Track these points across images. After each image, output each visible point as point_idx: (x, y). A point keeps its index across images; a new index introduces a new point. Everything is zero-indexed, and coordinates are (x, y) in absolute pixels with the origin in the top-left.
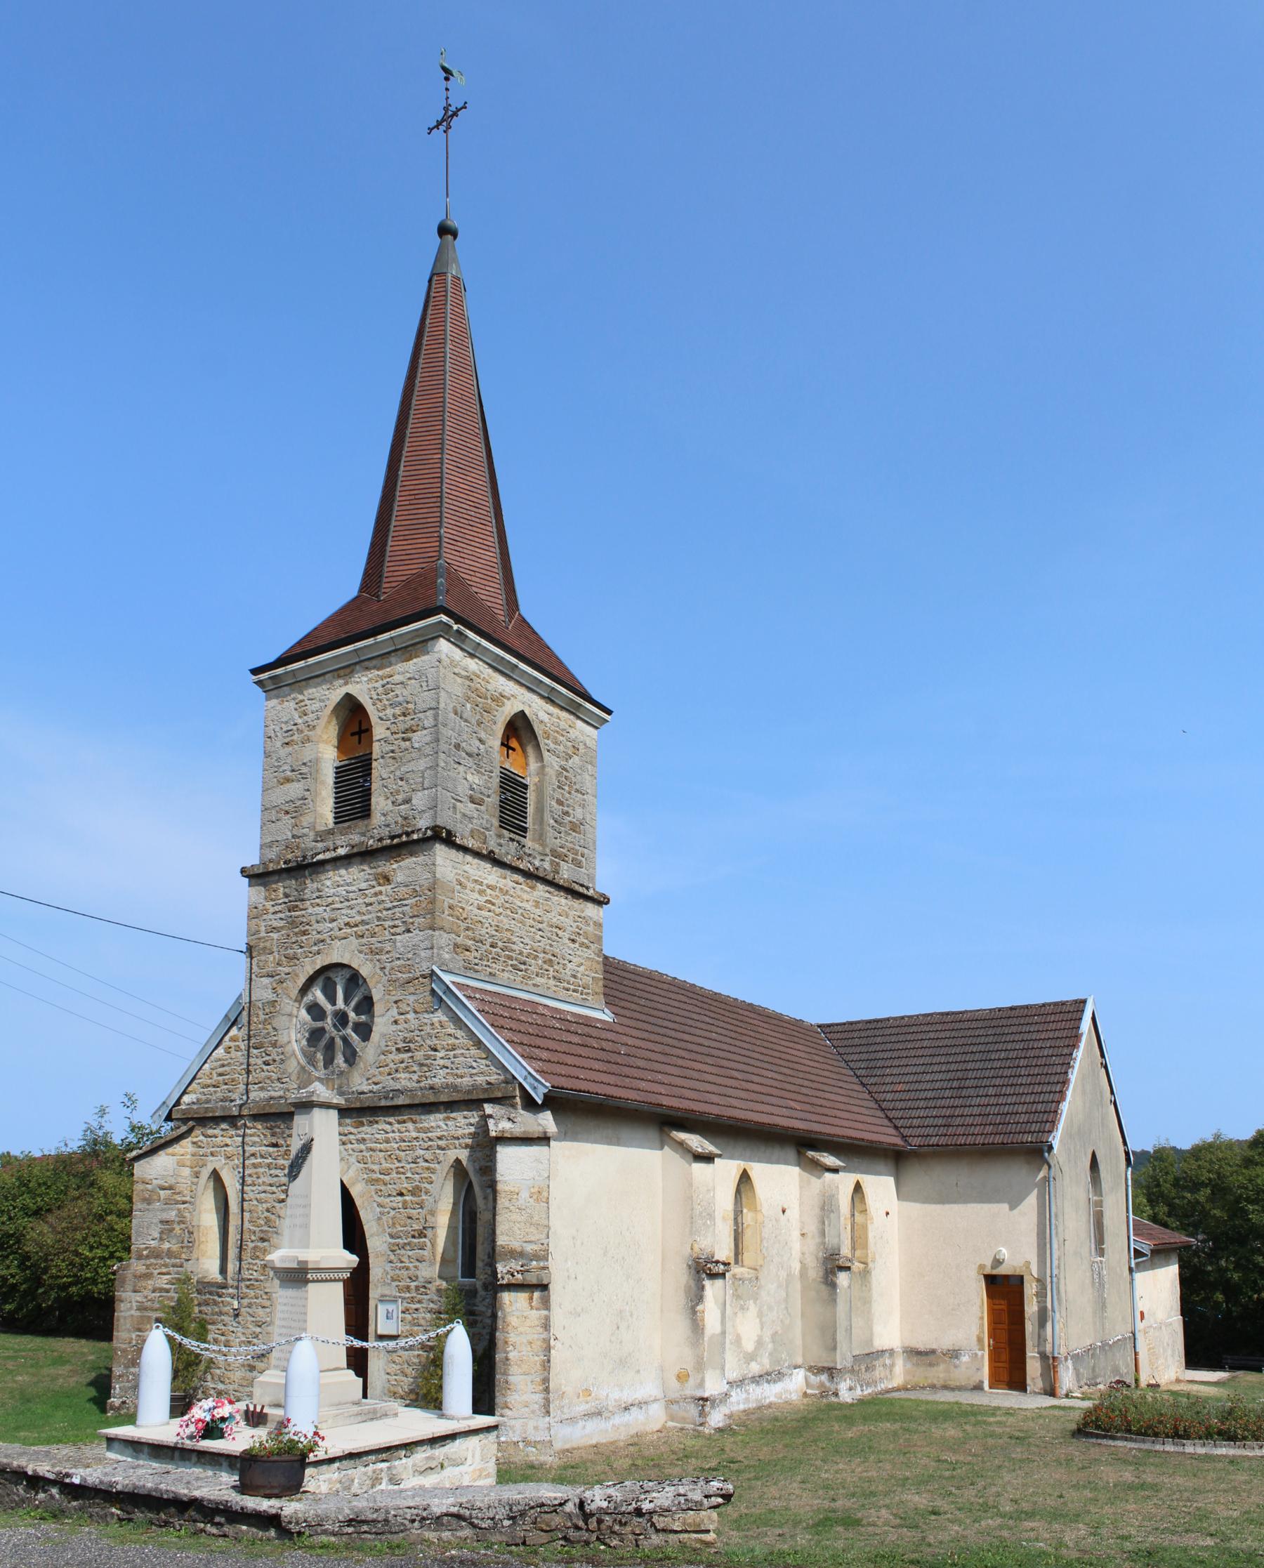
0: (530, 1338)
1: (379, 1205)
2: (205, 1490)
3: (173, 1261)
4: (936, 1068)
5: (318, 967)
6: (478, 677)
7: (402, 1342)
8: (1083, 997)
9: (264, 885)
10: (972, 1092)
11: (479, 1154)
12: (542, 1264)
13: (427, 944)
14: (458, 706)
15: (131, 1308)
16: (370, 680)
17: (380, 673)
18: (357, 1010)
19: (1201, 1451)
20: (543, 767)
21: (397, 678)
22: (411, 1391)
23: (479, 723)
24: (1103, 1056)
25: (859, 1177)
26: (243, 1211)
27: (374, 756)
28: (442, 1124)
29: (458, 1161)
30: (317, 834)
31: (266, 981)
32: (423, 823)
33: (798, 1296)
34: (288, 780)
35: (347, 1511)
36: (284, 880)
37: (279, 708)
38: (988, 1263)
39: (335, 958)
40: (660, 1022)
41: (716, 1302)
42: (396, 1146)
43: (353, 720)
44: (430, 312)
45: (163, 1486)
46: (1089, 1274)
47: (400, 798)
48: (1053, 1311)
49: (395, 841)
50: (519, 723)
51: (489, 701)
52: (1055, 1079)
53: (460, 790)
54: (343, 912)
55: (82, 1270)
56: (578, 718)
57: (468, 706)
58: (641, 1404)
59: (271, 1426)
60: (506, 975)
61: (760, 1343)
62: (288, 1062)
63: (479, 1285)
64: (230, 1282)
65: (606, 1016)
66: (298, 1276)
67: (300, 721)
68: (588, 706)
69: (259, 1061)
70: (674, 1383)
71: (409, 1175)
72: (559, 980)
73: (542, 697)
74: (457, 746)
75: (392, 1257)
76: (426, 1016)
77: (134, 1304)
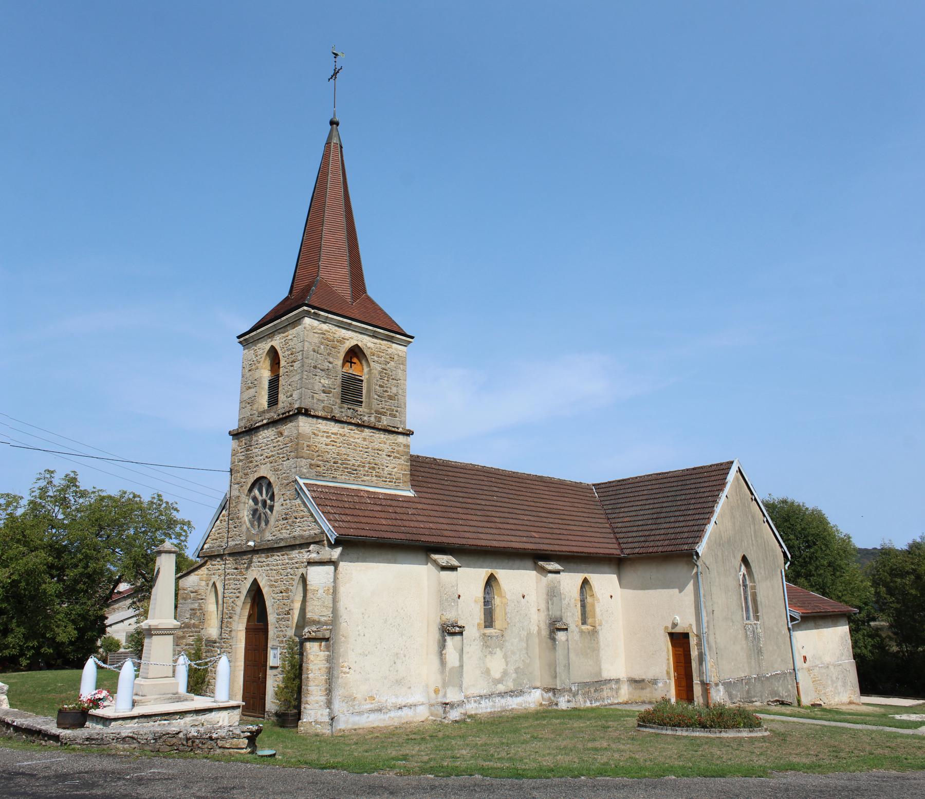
4: (647, 507)
19: (685, 734)
21: (290, 337)
23: (329, 354)
25: (586, 575)
31: (236, 486)
34: (250, 388)
38: (670, 625)
52: (707, 510)
53: (316, 388)
61: (505, 673)
65: (410, 494)
68: (398, 336)
70: (433, 695)
74: (315, 367)
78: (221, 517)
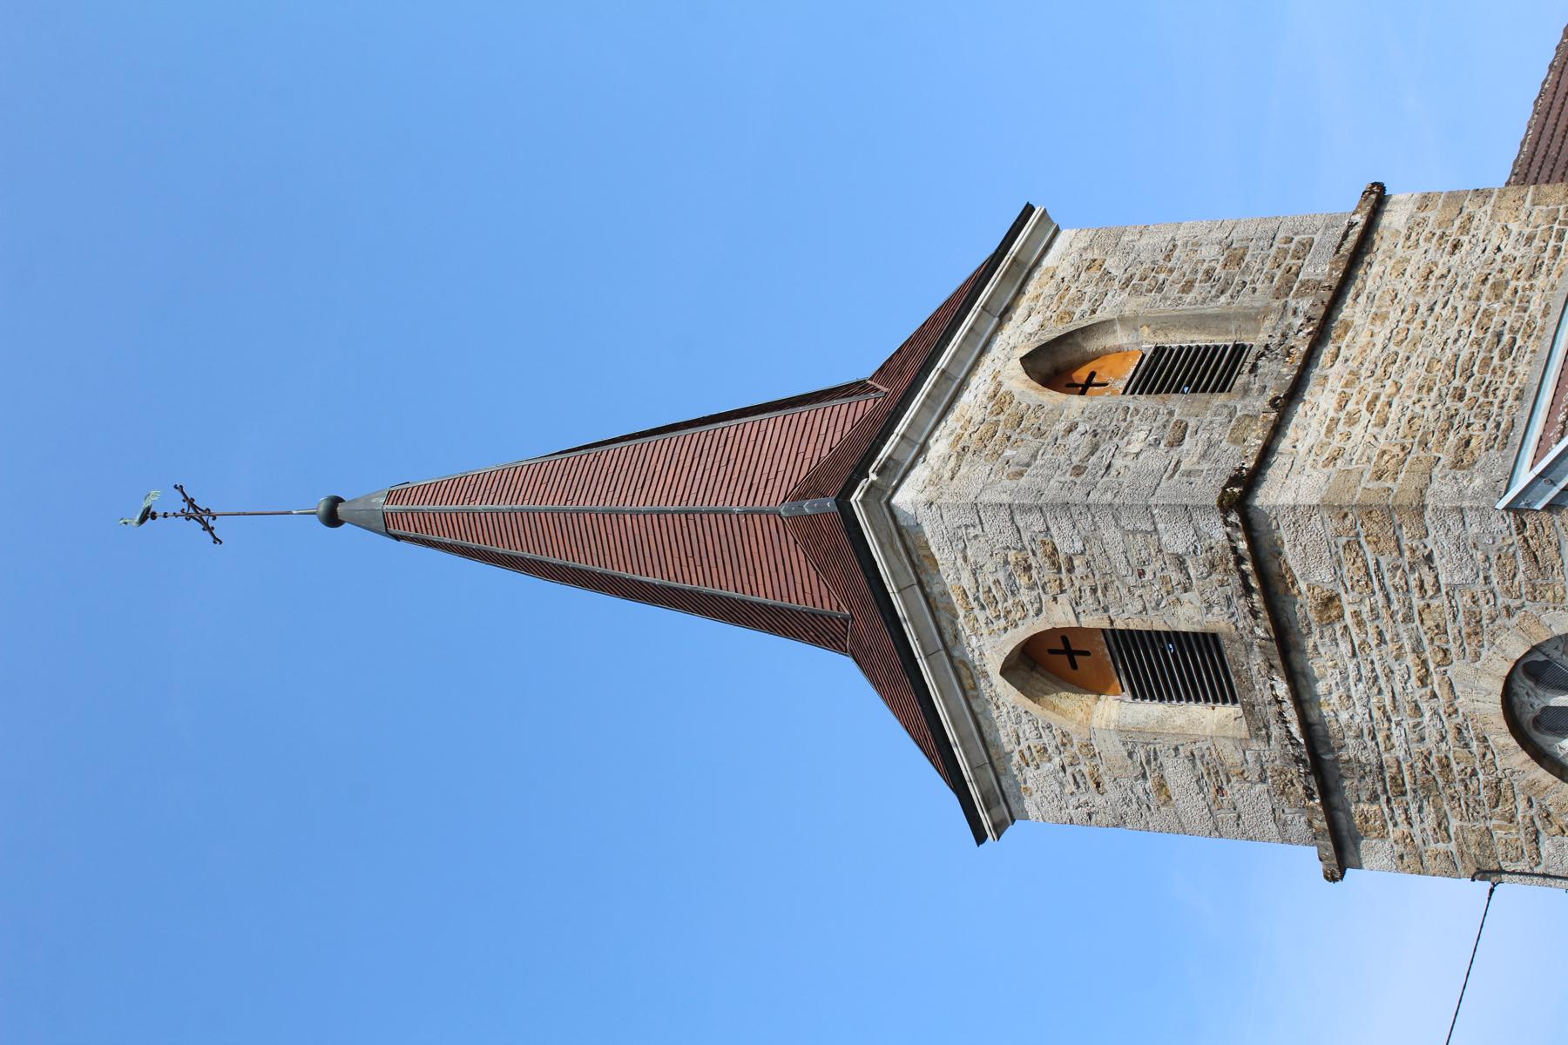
5: (1512, 742)
6: (960, 437)
9: (1357, 839)
14: (1008, 470)
16: (975, 631)
17: (961, 613)
20: (1123, 320)
21: (967, 581)
23: (1040, 433)
27: (1106, 625)
31: (1546, 847)
32: (1217, 531)
34: (1162, 786)
37: (1037, 796)
39: (1492, 708)
43: (1047, 662)
44: (435, 538)
47: (1176, 576)
49: (1254, 584)
50: (1045, 366)
51: (1002, 417)
54: (1398, 689)
57: (1008, 453)
60: (1521, 369)
67: (1057, 760)
72: (1537, 267)
73: (999, 327)
74: (1078, 470)
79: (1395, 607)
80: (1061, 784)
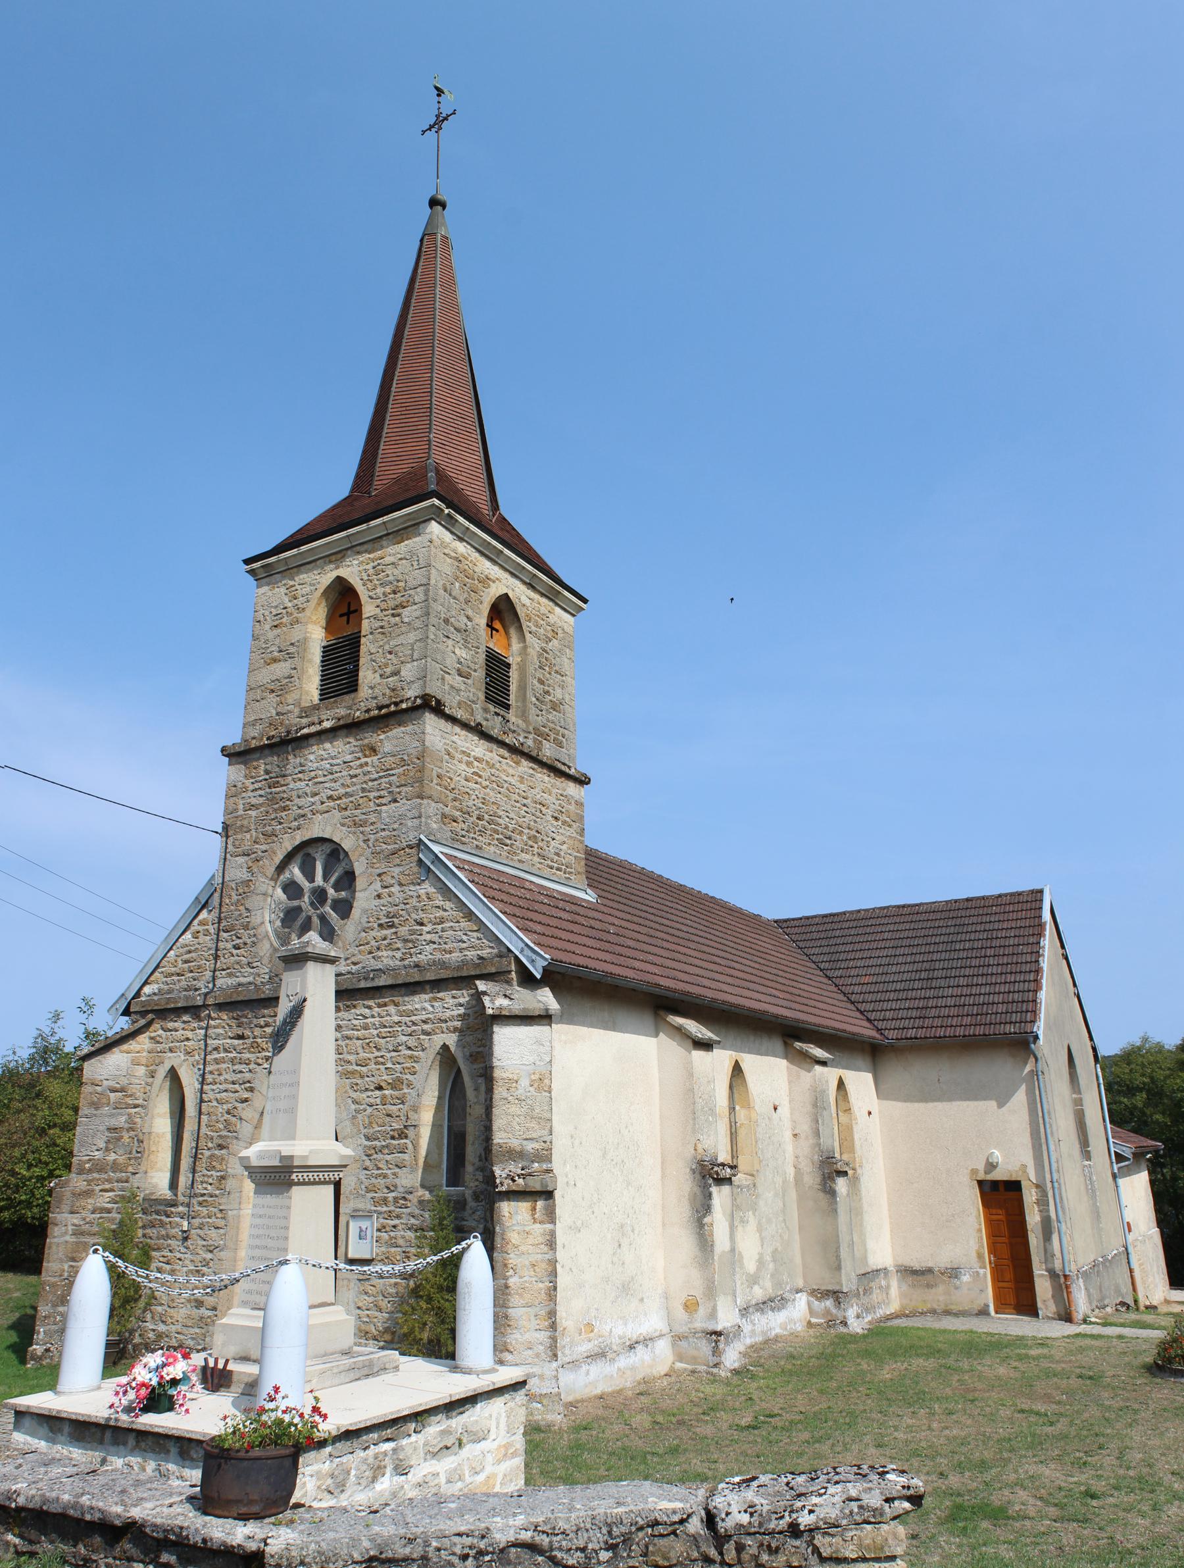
0: (533, 1258)
1: (355, 1102)
2: (149, 1505)
3: (119, 1175)
4: (900, 960)
5: (297, 843)
6: (466, 559)
7: (378, 1268)
8: (1038, 887)
9: (245, 763)
10: (943, 983)
11: (469, 1039)
12: (545, 1166)
13: (415, 813)
15: (66, 1233)
17: (371, 556)
18: (337, 887)
20: (525, 647)
21: (388, 560)
22: (387, 1330)
23: (467, 602)
24: (1063, 947)
26: (200, 1113)
27: (363, 633)
28: (427, 1005)
29: (445, 1047)
30: (303, 710)
31: (241, 860)
32: (412, 692)
33: (795, 1207)
34: (275, 660)
35: (366, 1544)
36: (266, 757)
37: (270, 593)
38: (981, 1167)
39: (316, 833)
40: (639, 906)
41: (724, 1214)
42: (375, 1032)
43: (344, 602)
45: (85, 1500)
46: (1082, 1179)
47: (388, 670)
48: (1058, 1221)
50: (503, 606)
53: (448, 662)
54: (327, 785)
55: (17, 1192)
56: (557, 604)
57: (457, 585)
58: (647, 1341)
59: (236, 1388)
60: (492, 848)
61: (761, 1262)
62: (259, 945)
63: (468, 1194)
64: (181, 1198)
65: (590, 896)
66: (278, 1177)
67: (290, 605)
68: (566, 593)
69: (229, 945)
70: (680, 1313)
71: (389, 1065)
72: (543, 857)
73: (524, 583)
74: (446, 621)
75: (368, 1163)
76: (412, 888)
77: (70, 1228)
78: (195, 926)
79: (370, 784)
80: (276, 607)
